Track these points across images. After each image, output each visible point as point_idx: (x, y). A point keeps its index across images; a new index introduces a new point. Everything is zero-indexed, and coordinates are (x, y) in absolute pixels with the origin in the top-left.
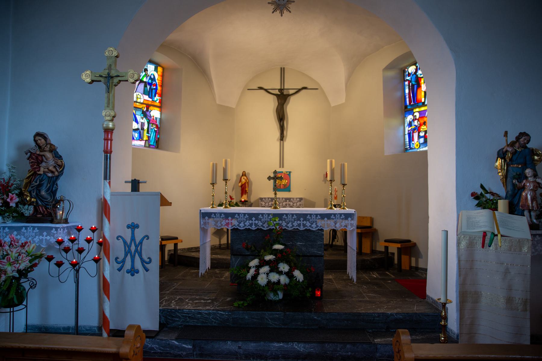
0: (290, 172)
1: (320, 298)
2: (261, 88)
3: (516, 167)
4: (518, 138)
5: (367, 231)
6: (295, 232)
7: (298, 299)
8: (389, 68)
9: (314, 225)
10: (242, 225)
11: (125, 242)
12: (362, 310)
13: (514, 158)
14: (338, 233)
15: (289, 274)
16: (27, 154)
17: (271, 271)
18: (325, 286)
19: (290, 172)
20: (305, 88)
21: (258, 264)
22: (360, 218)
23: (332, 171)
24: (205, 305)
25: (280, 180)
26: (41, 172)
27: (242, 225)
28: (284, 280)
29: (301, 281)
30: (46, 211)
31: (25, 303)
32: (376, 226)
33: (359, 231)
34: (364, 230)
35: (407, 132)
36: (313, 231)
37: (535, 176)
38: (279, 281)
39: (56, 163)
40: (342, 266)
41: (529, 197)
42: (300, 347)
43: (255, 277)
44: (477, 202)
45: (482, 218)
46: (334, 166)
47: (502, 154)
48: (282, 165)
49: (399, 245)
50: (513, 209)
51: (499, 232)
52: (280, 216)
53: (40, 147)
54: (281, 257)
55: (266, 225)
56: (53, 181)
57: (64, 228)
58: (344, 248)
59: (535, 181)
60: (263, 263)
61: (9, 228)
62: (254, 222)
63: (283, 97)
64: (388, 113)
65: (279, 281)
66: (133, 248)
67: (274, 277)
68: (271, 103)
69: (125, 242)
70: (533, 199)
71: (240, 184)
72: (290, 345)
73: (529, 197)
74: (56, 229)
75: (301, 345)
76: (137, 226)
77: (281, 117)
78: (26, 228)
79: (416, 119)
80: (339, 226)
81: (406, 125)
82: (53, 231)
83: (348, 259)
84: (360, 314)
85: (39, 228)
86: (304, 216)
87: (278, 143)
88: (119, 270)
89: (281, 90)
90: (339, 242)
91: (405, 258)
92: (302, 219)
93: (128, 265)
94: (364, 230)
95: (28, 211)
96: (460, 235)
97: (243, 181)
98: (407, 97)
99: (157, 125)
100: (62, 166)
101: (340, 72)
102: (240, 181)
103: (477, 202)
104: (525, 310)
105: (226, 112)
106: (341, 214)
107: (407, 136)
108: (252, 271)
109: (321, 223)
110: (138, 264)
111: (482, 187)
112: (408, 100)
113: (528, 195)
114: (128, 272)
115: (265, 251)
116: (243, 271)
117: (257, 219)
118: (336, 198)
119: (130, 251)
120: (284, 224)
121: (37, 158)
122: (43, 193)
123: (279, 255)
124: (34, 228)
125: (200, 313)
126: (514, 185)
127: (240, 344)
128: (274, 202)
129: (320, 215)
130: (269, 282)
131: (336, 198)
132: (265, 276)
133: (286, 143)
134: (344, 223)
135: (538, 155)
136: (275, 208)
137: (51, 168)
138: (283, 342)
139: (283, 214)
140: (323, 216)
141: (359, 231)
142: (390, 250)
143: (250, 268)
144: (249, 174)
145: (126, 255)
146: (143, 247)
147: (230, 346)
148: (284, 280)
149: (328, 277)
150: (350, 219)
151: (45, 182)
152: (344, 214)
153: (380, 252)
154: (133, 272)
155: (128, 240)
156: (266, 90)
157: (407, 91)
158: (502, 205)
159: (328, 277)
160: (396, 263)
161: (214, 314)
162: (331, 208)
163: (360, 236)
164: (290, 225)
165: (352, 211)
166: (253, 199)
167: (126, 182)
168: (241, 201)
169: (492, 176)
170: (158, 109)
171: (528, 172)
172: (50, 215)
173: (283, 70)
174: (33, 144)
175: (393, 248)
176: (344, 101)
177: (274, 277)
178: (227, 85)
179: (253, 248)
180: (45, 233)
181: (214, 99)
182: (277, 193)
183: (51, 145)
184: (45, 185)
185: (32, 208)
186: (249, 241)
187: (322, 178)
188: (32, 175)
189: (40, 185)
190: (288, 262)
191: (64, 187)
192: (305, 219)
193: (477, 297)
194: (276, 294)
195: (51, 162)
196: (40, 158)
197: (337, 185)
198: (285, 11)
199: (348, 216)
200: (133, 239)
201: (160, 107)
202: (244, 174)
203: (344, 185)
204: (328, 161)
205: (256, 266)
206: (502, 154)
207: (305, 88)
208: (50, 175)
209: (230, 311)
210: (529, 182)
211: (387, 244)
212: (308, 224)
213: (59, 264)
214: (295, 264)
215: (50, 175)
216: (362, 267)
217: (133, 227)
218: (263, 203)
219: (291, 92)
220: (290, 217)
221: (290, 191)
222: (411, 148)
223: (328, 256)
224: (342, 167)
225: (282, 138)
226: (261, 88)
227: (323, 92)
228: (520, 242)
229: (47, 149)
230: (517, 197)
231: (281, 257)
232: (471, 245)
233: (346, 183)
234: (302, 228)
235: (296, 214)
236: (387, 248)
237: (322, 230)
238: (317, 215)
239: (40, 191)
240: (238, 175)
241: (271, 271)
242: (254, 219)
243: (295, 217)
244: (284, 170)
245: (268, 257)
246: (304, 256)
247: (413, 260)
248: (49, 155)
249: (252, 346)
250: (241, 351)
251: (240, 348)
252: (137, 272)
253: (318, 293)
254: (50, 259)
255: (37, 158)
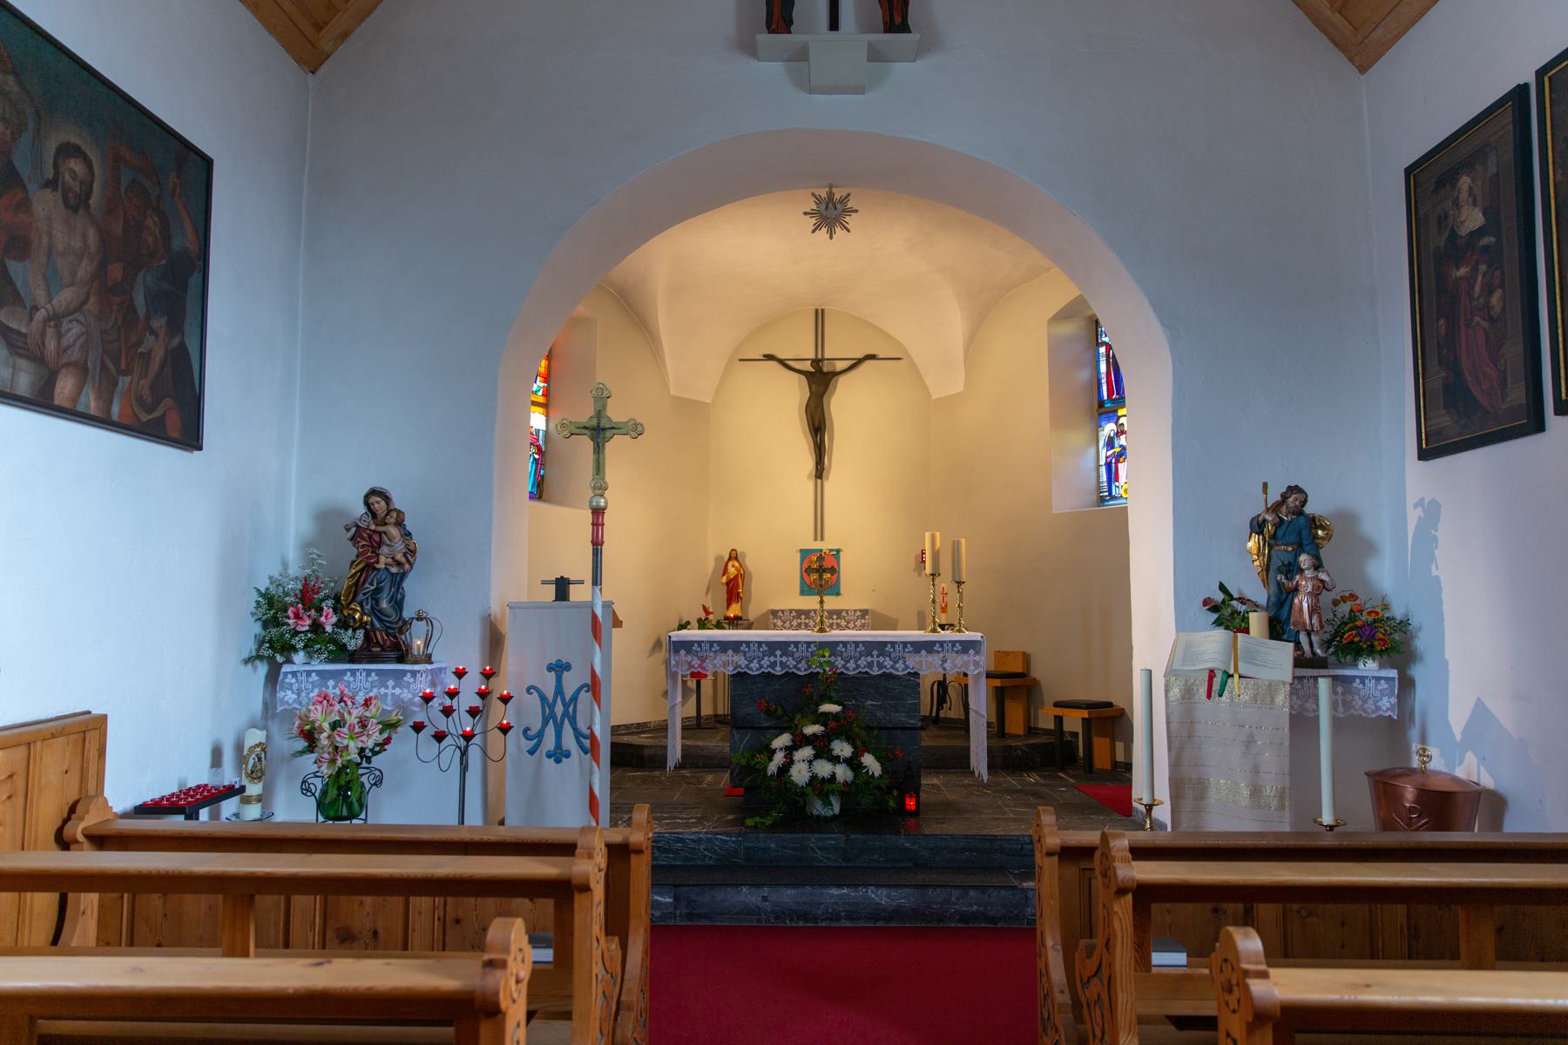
0: (838, 551)
1: (915, 814)
2: (769, 357)
3: (1283, 552)
4: (1284, 497)
5: (1014, 684)
6: (863, 680)
7: (875, 810)
8: (1062, 316)
9: (900, 665)
10: (754, 665)
11: (543, 698)
12: (998, 831)
13: (1280, 533)
14: (950, 690)
15: (854, 763)
16: (348, 530)
17: (817, 756)
18: (923, 796)
19: (838, 551)
20: (872, 357)
21: (789, 743)
22: (1001, 655)
23: (936, 556)
24: (687, 825)
25: (820, 572)
26: (381, 566)
27: (754, 665)
28: (843, 773)
29: (877, 774)
30: (388, 644)
31: (363, 816)
32: (1037, 672)
33: (998, 683)
34: (1008, 682)
35: (1102, 462)
36: (898, 677)
37: (1318, 566)
38: (833, 777)
39: (407, 546)
40: (958, 761)
41: (1305, 605)
42: (880, 896)
43: (785, 769)
44: (1215, 616)
45: (1212, 643)
46: (938, 545)
47: (1258, 526)
48: (819, 533)
49: (1085, 714)
50: (1277, 630)
51: (1236, 670)
52: (832, 646)
53: (374, 515)
54: (838, 727)
55: (803, 665)
56: (398, 581)
57: (426, 671)
58: (963, 725)
59: (1316, 578)
60: (800, 741)
61: (319, 673)
62: (390, 691)
63: (820, 379)
64: (1059, 420)
65: (833, 777)
66: (559, 709)
67: (824, 768)
68: (794, 392)
69: (543, 698)
70: (1312, 611)
71: (724, 579)
72: (861, 891)
73: (1305, 605)
74: (414, 673)
75: (884, 892)
76: (568, 667)
77: (817, 425)
78: (353, 672)
79: (1123, 432)
80: (954, 665)
81: (1101, 443)
82: (408, 678)
83: (973, 748)
84: (994, 838)
85: (378, 672)
86: (881, 646)
87: (811, 484)
88: (532, 752)
89: (816, 362)
90: (952, 712)
91: (1100, 744)
92: (875, 653)
93: (549, 742)
94: (1008, 682)
95: (354, 640)
96: (1170, 673)
97: (732, 571)
98: (1104, 381)
99: (539, 447)
100: (413, 552)
101: (955, 325)
102: (725, 571)
103: (1215, 616)
104: (1282, 807)
105: (693, 412)
106: (954, 643)
107: (1103, 470)
108: (779, 758)
109: (914, 661)
110: (569, 741)
111: (1222, 588)
112: (1105, 388)
113: (1303, 602)
114: (549, 756)
115: (804, 716)
116: (760, 758)
117: (689, 651)
118: (944, 610)
119: (552, 715)
120: (840, 663)
121: (370, 537)
122: (384, 605)
123: (832, 724)
124: (369, 672)
125: (681, 840)
126: (1279, 584)
127: (766, 891)
128: (800, 617)
129: (913, 643)
130: (814, 778)
131: (944, 610)
132: (804, 766)
133: (830, 485)
134: (961, 659)
135: (1323, 529)
136: (822, 630)
137: (399, 557)
138: (848, 886)
139: (837, 643)
140: (918, 646)
141: (998, 683)
142: (1067, 727)
143: (774, 752)
144: (744, 555)
145: (545, 723)
146: (579, 707)
147: (747, 896)
148: (843, 773)
149: (929, 780)
150: (972, 652)
151: (386, 585)
152: (961, 642)
153: (1047, 732)
154: (559, 755)
155: (550, 694)
156: (782, 362)
157: (1103, 368)
158: (1257, 621)
159: (929, 780)
160: (1076, 749)
161: (709, 840)
162: (934, 630)
163: (1000, 697)
164: (851, 665)
165: (976, 636)
166: (753, 613)
167: (544, 582)
168: (727, 618)
169: (1243, 568)
170: (541, 410)
171: (1304, 560)
172: (396, 646)
173: (820, 315)
174: (361, 509)
175: (1074, 722)
176: (961, 389)
177: (824, 768)
178: (692, 354)
179: (780, 711)
180: (391, 683)
181: (666, 386)
182: (825, 598)
183: (399, 512)
184: (386, 590)
185: (360, 634)
186: (777, 696)
187: (912, 564)
188: (362, 571)
189: (378, 590)
190: (850, 739)
191: (416, 594)
192: (882, 653)
193: (1201, 789)
194: (829, 804)
195: (399, 546)
196: (376, 538)
197: (945, 583)
198: (838, 230)
199: (967, 646)
200: (559, 691)
201: (545, 406)
202: (734, 556)
203: (959, 583)
204: (928, 535)
205: (787, 748)
206: (1258, 526)
207: (872, 357)
208: (394, 570)
209: (740, 834)
210: (1306, 579)
211: (1059, 711)
212: (888, 663)
213: (439, 737)
214: (864, 743)
215: (394, 570)
216: (1002, 760)
217: (559, 668)
218: (779, 623)
219: (840, 366)
220: (851, 648)
221: (838, 594)
222: (1113, 498)
223: (927, 739)
224: (956, 547)
225: (820, 472)
226: (769, 357)
227: (913, 367)
228: (1272, 688)
229: (391, 519)
230: (1286, 608)
231: (838, 727)
232: (1188, 693)
233: (964, 579)
234: (875, 672)
235: (864, 643)
236: (1059, 720)
237: (916, 675)
238: (905, 644)
239: (377, 601)
240: (718, 559)
241: (817, 756)
242: (778, 653)
243: (861, 648)
244: (824, 546)
245: (812, 729)
246: (881, 728)
247: (1120, 746)
248: (393, 531)
249: (788, 896)
250: (767, 906)
251: (765, 899)
252: (568, 755)
253: (911, 804)
254: (418, 727)
255: (370, 537)
